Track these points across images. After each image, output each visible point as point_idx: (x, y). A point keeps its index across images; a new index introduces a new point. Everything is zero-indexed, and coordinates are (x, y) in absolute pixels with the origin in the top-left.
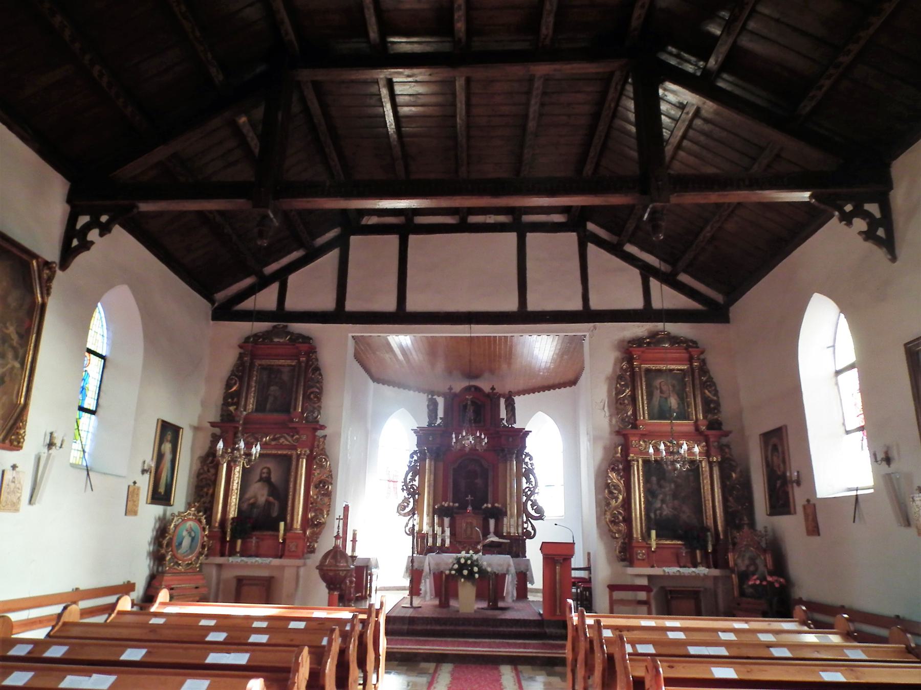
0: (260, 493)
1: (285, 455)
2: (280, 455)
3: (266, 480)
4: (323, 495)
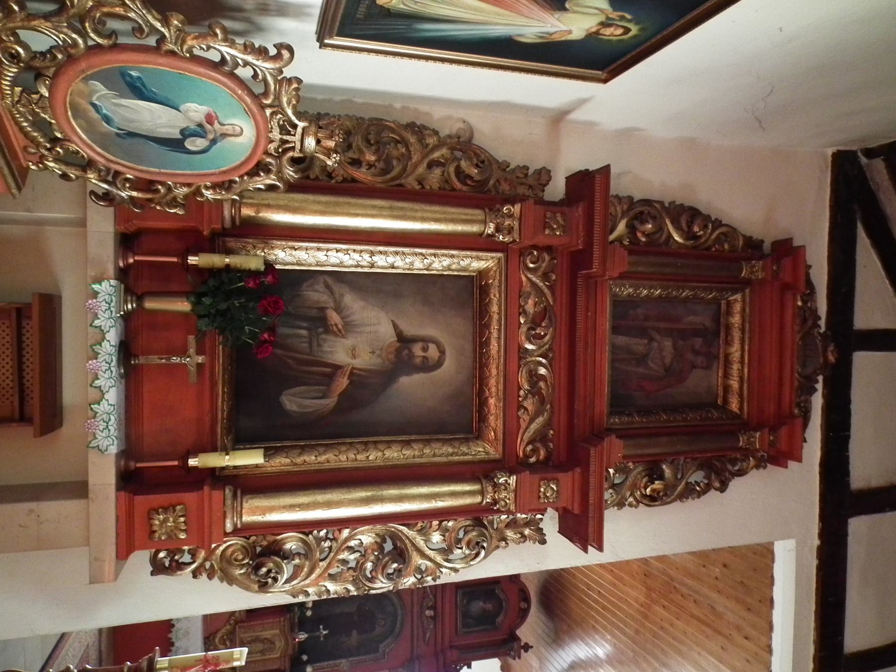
0: (360, 341)
1: (483, 418)
2: (483, 403)
3: (404, 355)
4: (359, 567)
